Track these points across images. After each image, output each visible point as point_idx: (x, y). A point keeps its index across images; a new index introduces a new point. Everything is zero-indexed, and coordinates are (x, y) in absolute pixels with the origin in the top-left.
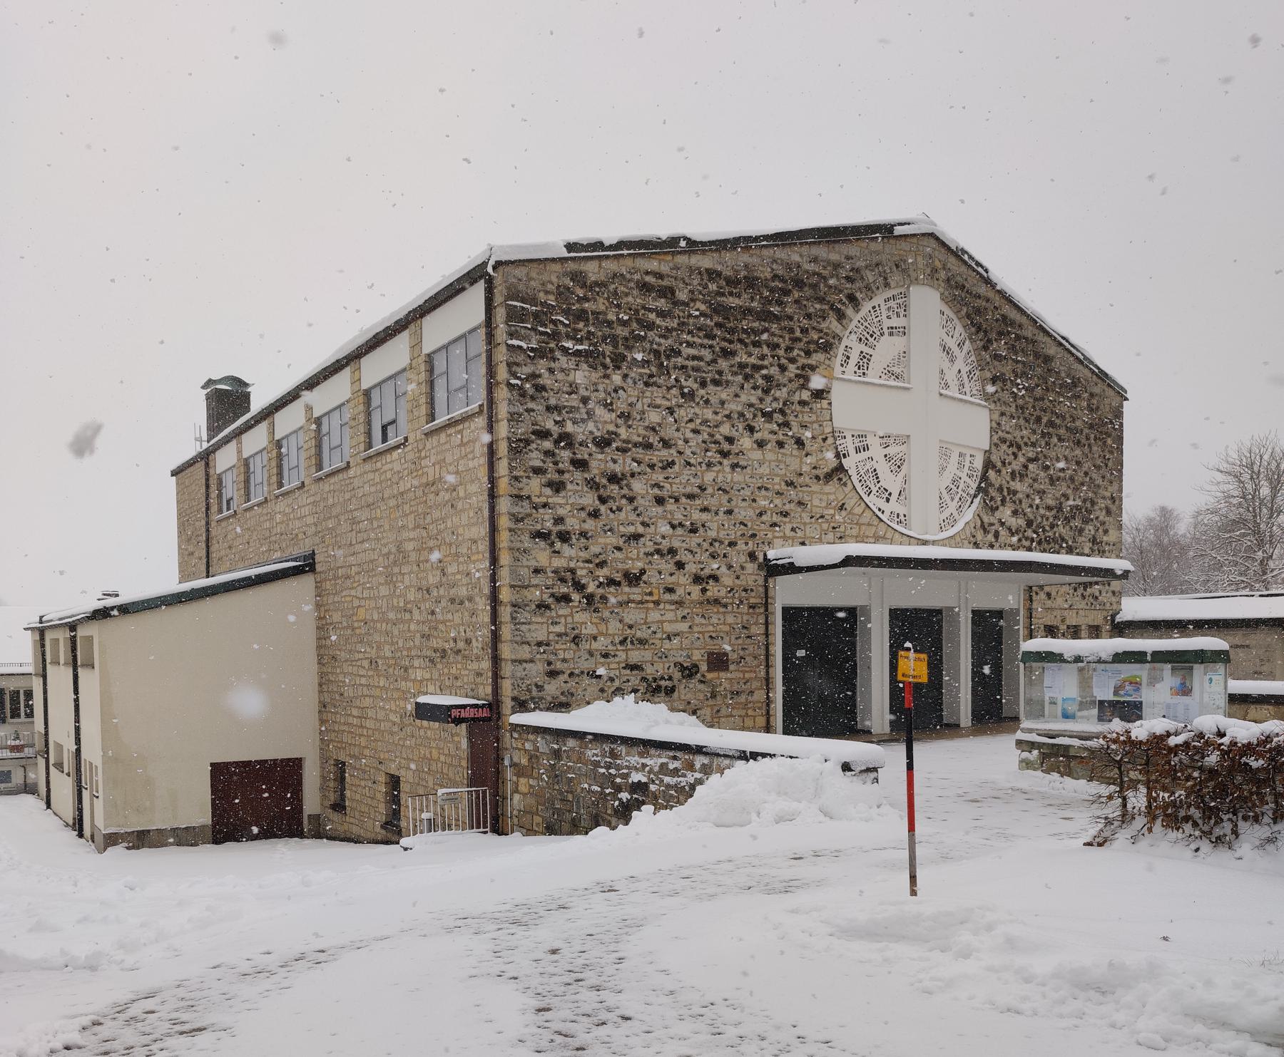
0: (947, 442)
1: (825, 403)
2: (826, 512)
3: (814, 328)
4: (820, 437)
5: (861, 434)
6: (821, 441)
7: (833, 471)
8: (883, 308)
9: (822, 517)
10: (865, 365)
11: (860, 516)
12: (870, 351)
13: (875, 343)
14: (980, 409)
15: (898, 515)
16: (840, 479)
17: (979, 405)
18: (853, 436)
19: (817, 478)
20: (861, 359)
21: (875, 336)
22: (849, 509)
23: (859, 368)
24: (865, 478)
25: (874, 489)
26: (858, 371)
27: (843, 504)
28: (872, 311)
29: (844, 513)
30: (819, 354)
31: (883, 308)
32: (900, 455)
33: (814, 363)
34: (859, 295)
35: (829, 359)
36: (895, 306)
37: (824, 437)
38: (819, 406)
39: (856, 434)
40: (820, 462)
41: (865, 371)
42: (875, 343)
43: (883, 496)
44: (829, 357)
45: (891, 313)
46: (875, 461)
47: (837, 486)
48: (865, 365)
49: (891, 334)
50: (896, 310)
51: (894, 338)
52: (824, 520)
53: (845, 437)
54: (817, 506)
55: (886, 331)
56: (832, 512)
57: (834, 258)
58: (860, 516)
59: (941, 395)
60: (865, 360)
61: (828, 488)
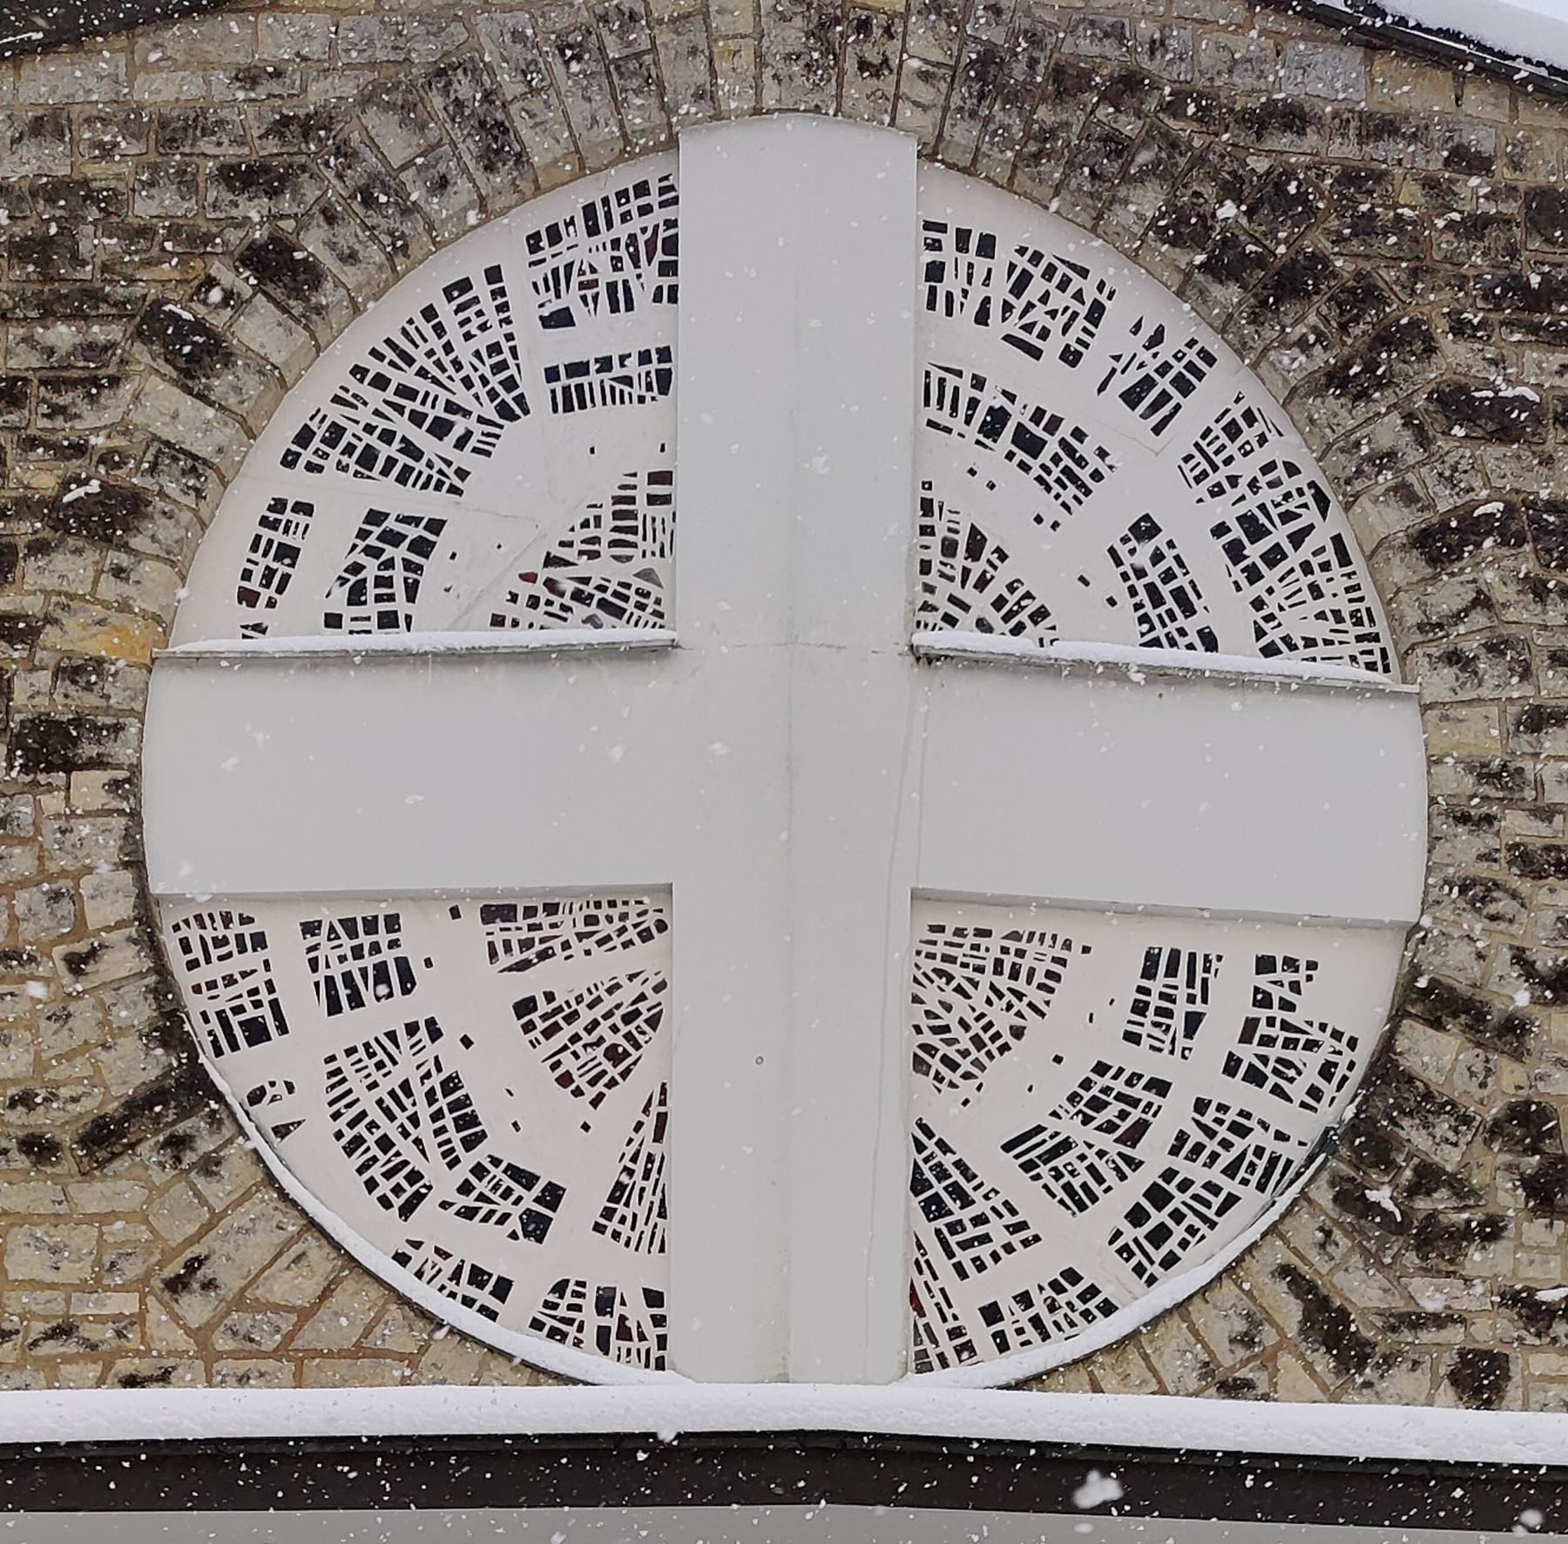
0: (1288, 921)
1: (89, 787)
2: (86, 1307)
3: (31, 443)
4: (59, 951)
5: (359, 913)
6: (62, 967)
7: (139, 1106)
8: (520, 278)
9: (63, 1331)
10: (398, 574)
11: (305, 1315)
12: (430, 504)
13: (464, 459)
14: (1368, 710)
15: (605, 1302)
16: (178, 1144)
17: (1356, 691)
18: (310, 928)
19: (39, 1148)
20: (371, 551)
21: (460, 425)
22: (231, 1282)
23: (356, 596)
24: (389, 1129)
25: (443, 1181)
26: (348, 612)
27: (193, 1265)
28: (446, 311)
29: (196, 1308)
30: (61, 561)
31: (520, 278)
32: (627, 995)
33: (33, 605)
34: (313, 244)
35: (119, 572)
36: (603, 260)
37: (82, 947)
38: (53, 803)
39: (329, 916)
40: (59, 1072)
41: (401, 606)
42: (464, 459)
43: (504, 1206)
44: (124, 560)
45: (570, 298)
46: (450, 1039)
47: (158, 1177)
48: (398, 574)
49: (572, 401)
50: (606, 275)
51: (595, 419)
52: (71, 1348)
53: (259, 941)
54: (34, 1284)
55: (534, 387)
56: (127, 1304)
57: (169, 94)
58: (305, 1315)
59: (927, 659)
60: (400, 553)
61: (92, 1196)
